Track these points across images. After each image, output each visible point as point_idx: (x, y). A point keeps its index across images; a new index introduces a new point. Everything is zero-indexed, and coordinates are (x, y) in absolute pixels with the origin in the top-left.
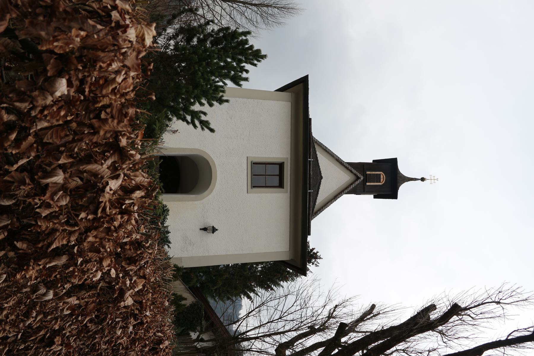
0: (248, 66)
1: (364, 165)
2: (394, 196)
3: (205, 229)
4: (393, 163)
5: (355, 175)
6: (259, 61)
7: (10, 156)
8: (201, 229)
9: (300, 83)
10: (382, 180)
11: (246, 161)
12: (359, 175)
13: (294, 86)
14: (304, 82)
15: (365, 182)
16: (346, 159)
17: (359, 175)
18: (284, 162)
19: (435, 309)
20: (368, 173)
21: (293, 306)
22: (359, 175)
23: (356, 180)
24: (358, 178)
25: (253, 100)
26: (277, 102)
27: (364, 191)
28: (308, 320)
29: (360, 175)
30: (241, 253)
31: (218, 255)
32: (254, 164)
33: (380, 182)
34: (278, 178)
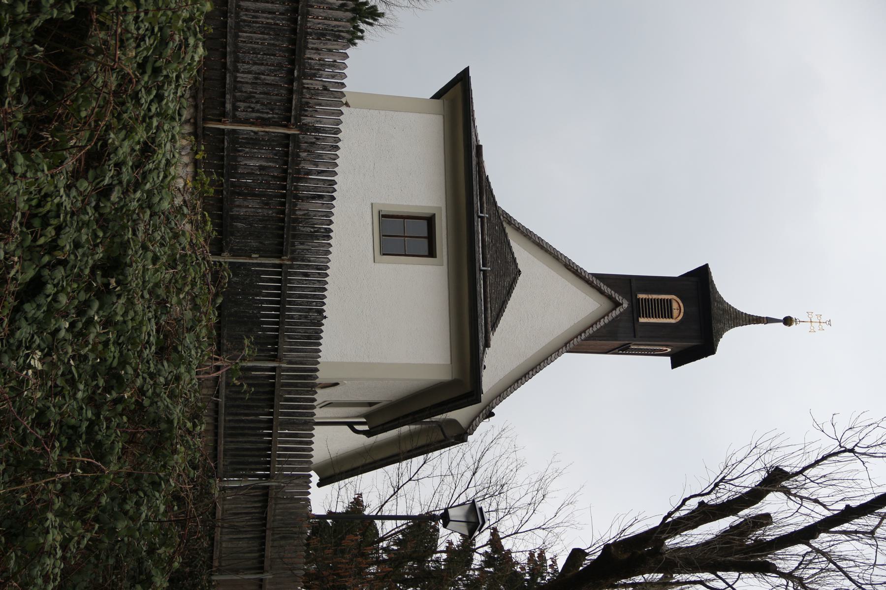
0: (362, 26)
1: (630, 280)
5: (610, 297)
6: (375, 20)
9: (458, 82)
10: (675, 313)
11: (369, 210)
12: (617, 299)
13: (447, 92)
14: (463, 80)
15: (635, 316)
16: (591, 267)
17: (619, 298)
18: (434, 215)
19: (771, 523)
20: (641, 296)
21: (468, 488)
22: (619, 298)
23: (614, 309)
24: (617, 304)
25: (377, 111)
26: (418, 115)
29: (620, 297)
30: (367, 361)
31: (327, 362)
32: (385, 217)
33: (672, 317)
34: (425, 241)
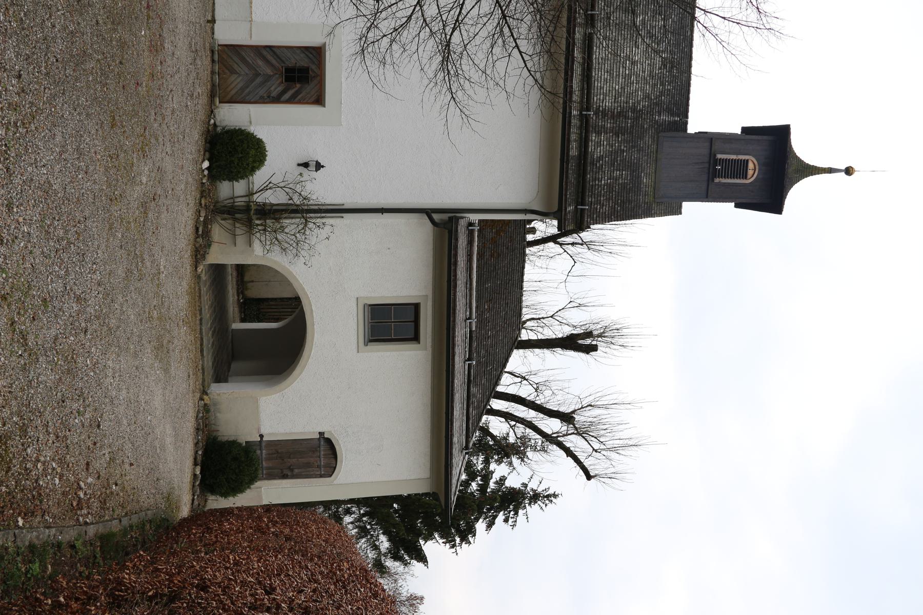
3: (306, 165)
4: (781, 134)
8: (299, 165)
10: (750, 172)
20: (719, 156)
28: (410, 37)
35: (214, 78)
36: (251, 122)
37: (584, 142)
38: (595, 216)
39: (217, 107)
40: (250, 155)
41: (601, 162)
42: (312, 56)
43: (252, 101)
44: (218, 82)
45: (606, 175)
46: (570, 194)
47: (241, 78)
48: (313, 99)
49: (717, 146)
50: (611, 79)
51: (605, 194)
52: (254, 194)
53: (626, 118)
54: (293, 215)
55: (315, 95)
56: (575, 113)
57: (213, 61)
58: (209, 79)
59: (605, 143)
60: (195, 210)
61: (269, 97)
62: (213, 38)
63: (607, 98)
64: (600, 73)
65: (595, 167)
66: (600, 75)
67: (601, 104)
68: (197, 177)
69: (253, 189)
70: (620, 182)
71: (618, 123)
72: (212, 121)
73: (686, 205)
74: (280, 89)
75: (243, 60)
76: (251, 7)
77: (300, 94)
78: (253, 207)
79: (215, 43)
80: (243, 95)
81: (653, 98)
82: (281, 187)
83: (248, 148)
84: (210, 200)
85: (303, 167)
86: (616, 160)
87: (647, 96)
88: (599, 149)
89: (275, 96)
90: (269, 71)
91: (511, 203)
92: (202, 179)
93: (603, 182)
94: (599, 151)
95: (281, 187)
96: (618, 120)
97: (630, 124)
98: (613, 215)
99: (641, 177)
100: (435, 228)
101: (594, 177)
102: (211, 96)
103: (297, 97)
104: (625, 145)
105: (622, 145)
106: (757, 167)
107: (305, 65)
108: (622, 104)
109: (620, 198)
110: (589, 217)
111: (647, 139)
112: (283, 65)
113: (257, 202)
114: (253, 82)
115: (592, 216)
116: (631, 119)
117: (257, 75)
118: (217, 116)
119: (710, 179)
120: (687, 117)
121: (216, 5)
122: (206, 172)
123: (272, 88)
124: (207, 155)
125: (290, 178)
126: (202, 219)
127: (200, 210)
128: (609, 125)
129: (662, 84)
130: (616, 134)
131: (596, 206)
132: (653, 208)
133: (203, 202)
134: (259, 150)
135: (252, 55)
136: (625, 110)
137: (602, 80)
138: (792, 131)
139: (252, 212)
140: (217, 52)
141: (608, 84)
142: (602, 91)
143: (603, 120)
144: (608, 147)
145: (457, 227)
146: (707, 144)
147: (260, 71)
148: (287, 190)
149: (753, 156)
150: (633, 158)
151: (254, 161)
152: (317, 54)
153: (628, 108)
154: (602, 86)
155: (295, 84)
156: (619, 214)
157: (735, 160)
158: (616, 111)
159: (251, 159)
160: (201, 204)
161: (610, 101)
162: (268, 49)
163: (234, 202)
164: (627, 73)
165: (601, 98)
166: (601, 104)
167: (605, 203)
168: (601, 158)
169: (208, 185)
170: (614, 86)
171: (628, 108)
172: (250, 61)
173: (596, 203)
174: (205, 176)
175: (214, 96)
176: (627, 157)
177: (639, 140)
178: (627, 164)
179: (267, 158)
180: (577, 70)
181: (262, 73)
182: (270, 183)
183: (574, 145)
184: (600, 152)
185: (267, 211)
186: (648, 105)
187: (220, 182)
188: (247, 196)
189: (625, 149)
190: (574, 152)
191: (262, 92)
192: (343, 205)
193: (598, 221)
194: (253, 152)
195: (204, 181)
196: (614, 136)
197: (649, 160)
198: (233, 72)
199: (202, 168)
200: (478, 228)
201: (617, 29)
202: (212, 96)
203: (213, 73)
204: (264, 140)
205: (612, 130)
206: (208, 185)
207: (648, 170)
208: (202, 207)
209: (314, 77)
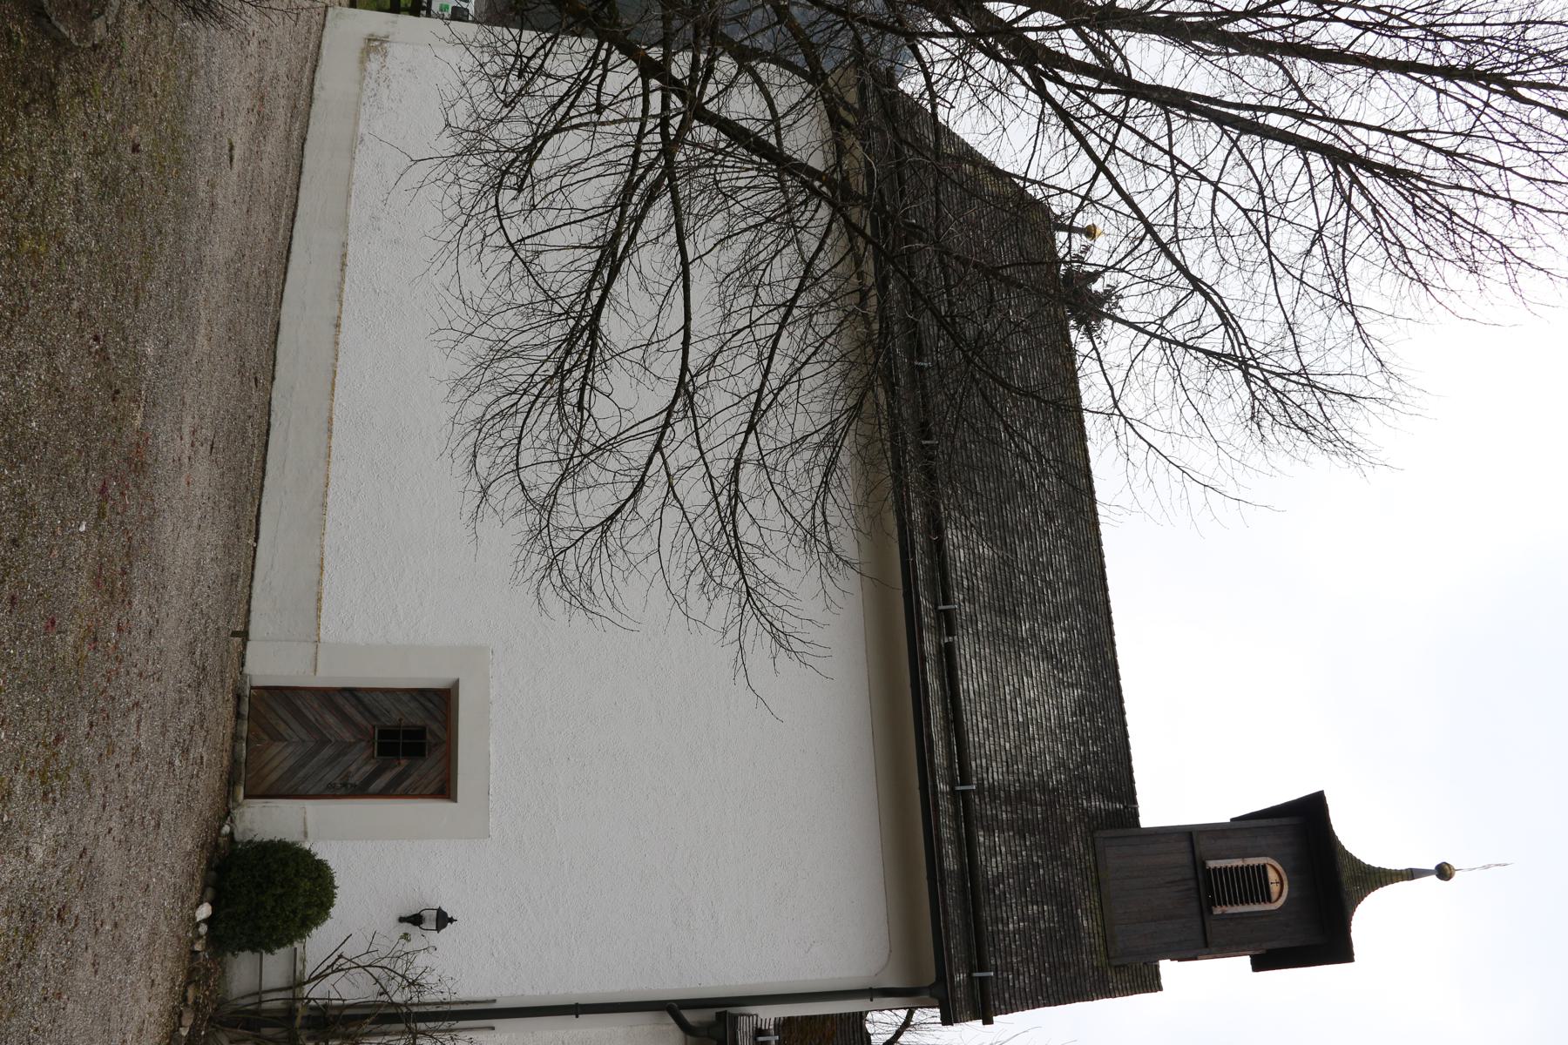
2: (1339, 950)
3: (416, 920)
7: (1388, 20)
8: (402, 920)
10: (1275, 889)
20: (1212, 864)
27: (1206, 945)
33: (1270, 900)
35: (237, 749)
36: (306, 834)
37: (967, 847)
38: (1007, 995)
39: (239, 805)
40: (301, 891)
41: (1001, 886)
42: (431, 705)
43: (311, 793)
44: (244, 755)
45: (1015, 912)
46: (956, 948)
47: (290, 749)
48: (432, 788)
49: (1203, 845)
50: (996, 731)
51: (1019, 951)
52: (305, 983)
53: (1033, 803)
54: (385, 1027)
55: (438, 779)
56: (942, 787)
57: (238, 715)
58: (227, 746)
59: (1003, 849)
60: (169, 1007)
61: (345, 785)
62: (241, 673)
63: (994, 764)
64: (974, 717)
65: (992, 896)
66: (976, 722)
67: (985, 775)
68: (181, 932)
69: (302, 973)
70: (1042, 926)
71: (1019, 811)
72: (226, 829)
73: (1168, 969)
74: (368, 768)
75: (298, 714)
76: (319, 617)
77: (408, 778)
78: (302, 1011)
79: (246, 682)
80: (292, 783)
81: (1071, 766)
82: (363, 967)
83: (295, 876)
84: (207, 993)
85: (410, 925)
86: (1027, 883)
87: (1061, 764)
88: (994, 860)
89: (357, 783)
90: (347, 736)
91: (840, 978)
92: (193, 944)
93: (1011, 926)
94: (994, 865)
95: (363, 967)
96: (1019, 807)
97: (1042, 814)
98: (1039, 993)
99: (1078, 917)
100: (689, 1037)
101: (993, 915)
102: (229, 783)
103: (399, 785)
104: (1040, 854)
105: (1034, 853)
106: (1284, 877)
107: (419, 723)
108: (1021, 778)
109: (1046, 958)
110: (996, 997)
111: (1075, 843)
112: (375, 723)
113: (310, 1000)
114: (314, 757)
115: (1001, 996)
116: (1041, 805)
117: (323, 742)
118: (237, 822)
119: (1205, 911)
120: (1135, 802)
121: (253, 614)
122: (203, 929)
123: (353, 768)
124: (210, 893)
125: (384, 946)
126: (184, 1032)
127: (181, 1012)
128: (1004, 816)
129: (1083, 743)
130: (1019, 833)
131: (1005, 975)
132: (1110, 979)
133: (191, 993)
134: (320, 880)
135: (316, 706)
136: (1028, 788)
137: (981, 732)
138: (1329, 801)
139: (298, 1022)
140: (247, 699)
141: (991, 739)
142: (983, 752)
143: (993, 805)
144: (1009, 858)
145: (735, 1034)
146: (1185, 844)
147: (328, 736)
148: (376, 972)
149: (1274, 857)
150: (1056, 879)
151: (308, 905)
152: (441, 702)
153: (1032, 785)
154: (982, 742)
155: (399, 759)
156: (1050, 992)
157: (1242, 868)
158: (1012, 789)
159: (301, 900)
160: (185, 999)
161: (1000, 770)
162: (347, 694)
163: (261, 1002)
164: (1021, 720)
165: (984, 764)
166: (985, 775)
167: (1021, 969)
168: (999, 879)
169: (205, 959)
170: (1002, 743)
171: (1032, 785)
172: (311, 717)
173: (1004, 968)
174: (200, 937)
175: (234, 783)
176: (1047, 877)
177: (1062, 846)
178: (1048, 891)
179: (336, 901)
180: (936, 712)
181: (333, 739)
182: (340, 956)
183: (949, 849)
184: (997, 867)
185: (331, 1019)
186: (1065, 779)
187: (233, 954)
188: (290, 988)
189: (1040, 861)
190: (950, 864)
191: (331, 775)
192: (494, 1001)
193: (1014, 1007)
194: (306, 884)
195: (198, 947)
196: (1017, 837)
197: (1085, 883)
198: (276, 737)
199: (194, 919)
200: (777, 1038)
201: (992, 643)
202: (231, 782)
203: (236, 737)
204: (332, 864)
205: (1011, 825)
206: (205, 959)
207: (1088, 903)
208: (186, 1005)
209: (436, 745)
